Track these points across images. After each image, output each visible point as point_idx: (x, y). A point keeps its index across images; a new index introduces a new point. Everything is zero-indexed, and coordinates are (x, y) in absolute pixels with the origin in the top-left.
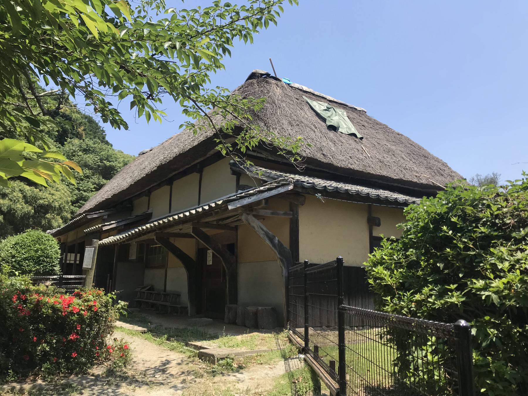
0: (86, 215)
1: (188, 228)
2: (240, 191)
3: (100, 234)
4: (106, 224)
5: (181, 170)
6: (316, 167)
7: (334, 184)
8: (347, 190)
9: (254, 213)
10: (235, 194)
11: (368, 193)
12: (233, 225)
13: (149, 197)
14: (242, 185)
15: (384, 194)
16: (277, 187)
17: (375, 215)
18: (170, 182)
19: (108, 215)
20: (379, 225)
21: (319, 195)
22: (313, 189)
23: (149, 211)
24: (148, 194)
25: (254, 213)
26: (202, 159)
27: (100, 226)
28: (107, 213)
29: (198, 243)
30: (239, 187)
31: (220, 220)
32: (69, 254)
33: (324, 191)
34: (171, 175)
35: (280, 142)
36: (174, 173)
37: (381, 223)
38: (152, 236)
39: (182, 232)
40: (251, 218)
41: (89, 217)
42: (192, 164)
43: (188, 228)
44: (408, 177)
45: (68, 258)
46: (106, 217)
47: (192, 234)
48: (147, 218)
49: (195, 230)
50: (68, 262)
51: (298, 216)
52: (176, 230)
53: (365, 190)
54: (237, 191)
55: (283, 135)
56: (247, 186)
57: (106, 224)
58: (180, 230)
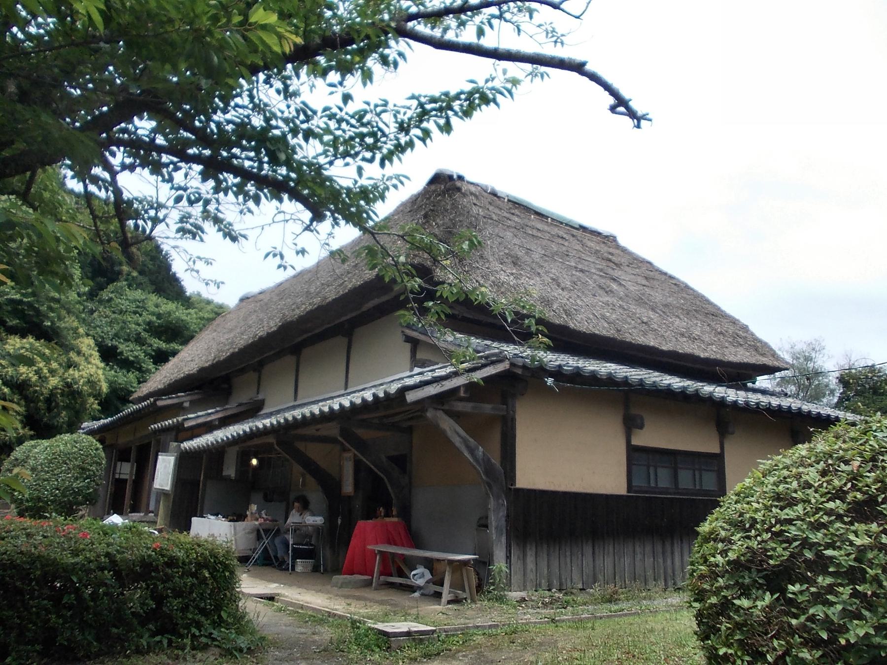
0: (155, 401)
1: (332, 430)
2: (417, 370)
3: (182, 433)
4: (190, 416)
5: (317, 331)
6: (565, 339)
7: (687, 383)
8: (593, 372)
9: (446, 407)
10: (408, 373)
11: (626, 377)
12: (405, 425)
13: (260, 372)
14: (420, 360)
15: (635, 374)
16: (484, 366)
17: (634, 411)
18: (296, 350)
19: (191, 402)
20: (641, 427)
21: (550, 381)
22: (542, 371)
23: (260, 397)
24: (259, 367)
25: (446, 407)
26: (354, 314)
27: (180, 419)
28: (188, 398)
29: (355, 455)
30: (416, 362)
31: (385, 416)
32: (119, 463)
33: (558, 373)
34: (300, 339)
35: (486, 293)
36: (305, 336)
37: (646, 426)
38: (271, 439)
39: (319, 433)
40: (440, 414)
41: (160, 403)
42: (336, 322)
43: (332, 430)
44: (686, 347)
45: (118, 471)
46: (187, 405)
47: (340, 438)
48: (253, 410)
49: (345, 433)
50: (117, 476)
51: (514, 412)
52: (310, 431)
53: (676, 382)
54: (411, 370)
55: (497, 282)
56: (430, 361)
57: (190, 416)
58: (317, 430)
